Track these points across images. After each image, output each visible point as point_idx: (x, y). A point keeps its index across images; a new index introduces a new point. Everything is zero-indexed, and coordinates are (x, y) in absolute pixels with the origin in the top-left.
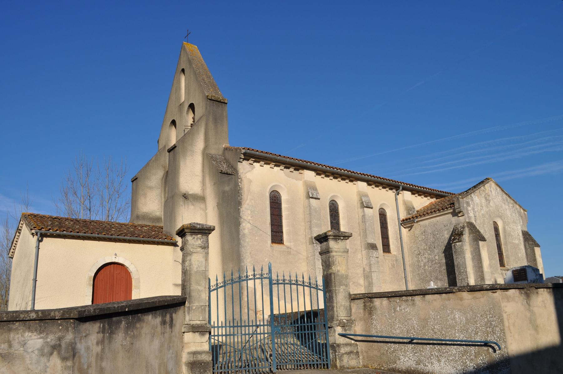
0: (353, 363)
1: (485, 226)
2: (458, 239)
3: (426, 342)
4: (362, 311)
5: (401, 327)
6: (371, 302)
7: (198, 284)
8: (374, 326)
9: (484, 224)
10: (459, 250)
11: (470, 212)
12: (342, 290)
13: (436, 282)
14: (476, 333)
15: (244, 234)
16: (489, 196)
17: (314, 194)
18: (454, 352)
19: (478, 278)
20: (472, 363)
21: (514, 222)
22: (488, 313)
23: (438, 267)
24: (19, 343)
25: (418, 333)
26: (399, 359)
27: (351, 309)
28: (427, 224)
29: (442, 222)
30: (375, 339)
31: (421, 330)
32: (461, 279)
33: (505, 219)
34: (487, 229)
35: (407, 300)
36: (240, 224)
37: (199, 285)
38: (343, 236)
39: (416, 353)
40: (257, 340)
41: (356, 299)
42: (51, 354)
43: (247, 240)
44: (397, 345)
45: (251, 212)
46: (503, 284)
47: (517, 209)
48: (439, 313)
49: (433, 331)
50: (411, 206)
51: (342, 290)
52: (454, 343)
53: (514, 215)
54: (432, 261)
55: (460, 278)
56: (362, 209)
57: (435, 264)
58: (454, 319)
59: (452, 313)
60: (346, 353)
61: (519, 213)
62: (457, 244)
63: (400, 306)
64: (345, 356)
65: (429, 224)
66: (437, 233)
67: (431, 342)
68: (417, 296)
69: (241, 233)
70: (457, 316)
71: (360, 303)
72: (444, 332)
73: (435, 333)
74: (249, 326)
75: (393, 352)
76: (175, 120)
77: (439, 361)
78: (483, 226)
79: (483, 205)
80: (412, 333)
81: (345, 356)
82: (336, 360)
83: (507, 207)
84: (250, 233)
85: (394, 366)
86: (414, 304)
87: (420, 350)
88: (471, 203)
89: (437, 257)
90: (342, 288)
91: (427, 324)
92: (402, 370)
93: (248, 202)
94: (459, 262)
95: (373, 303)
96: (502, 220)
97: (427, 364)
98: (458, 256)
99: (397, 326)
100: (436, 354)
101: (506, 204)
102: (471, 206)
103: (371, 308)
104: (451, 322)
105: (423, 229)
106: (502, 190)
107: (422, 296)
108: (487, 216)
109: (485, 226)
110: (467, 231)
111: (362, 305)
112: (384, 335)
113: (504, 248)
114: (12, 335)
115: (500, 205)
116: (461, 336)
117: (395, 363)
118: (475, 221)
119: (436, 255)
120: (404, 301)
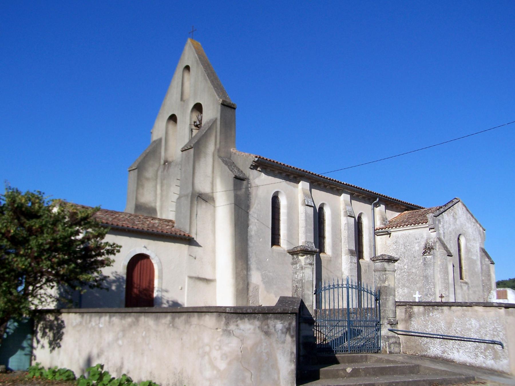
0: (396, 350)
1: (451, 242)
2: (429, 253)
3: (450, 338)
4: (403, 314)
5: (432, 327)
6: (411, 308)
7: (308, 289)
8: (413, 325)
9: (450, 240)
10: (429, 263)
11: (440, 229)
12: (391, 299)
13: (403, 289)
14: (486, 335)
15: (251, 236)
16: (456, 214)
17: (309, 201)
18: (470, 346)
19: (443, 289)
20: (481, 354)
21: (474, 240)
22: (495, 322)
23: (406, 276)
24: (272, 326)
25: (444, 332)
26: (430, 349)
27: (396, 312)
28: (400, 236)
29: (414, 235)
30: (412, 334)
31: (447, 330)
32: (428, 289)
33: (467, 236)
34: (452, 245)
35: (438, 309)
36: (248, 226)
37: (309, 291)
38: (393, 260)
39: (442, 345)
40: (339, 330)
41: (400, 306)
42: (286, 333)
43: (253, 241)
44: (428, 339)
45: (258, 215)
46: (52, 209)
47: (477, 227)
48: (460, 319)
49: (455, 331)
50: (384, 217)
51: (391, 299)
52: (469, 340)
53: (474, 233)
54: (401, 270)
55: (427, 288)
56: (345, 217)
57: (403, 273)
58: (471, 324)
59: (470, 320)
60: (392, 343)
61: (479, 231)
62: (428, 256)
63: (432, 313)
64: (392, 344)
65: (401, 235)
66: (408, 244)
67: (454, 338)
68: (445, 307)
69: (249, 235)
70: (473, 323)
71: (403, 309)
72: (463, 333)
73: (457, 333)
74: (334, 320)
75: (425, 344)
76: (177, 115)
77: (458, 352)
78: (450, 242)
79: (451, 223)
80: (440, 332)
81: (392, 344)
82: (386, 347)
83: (470, 226)
84: (256, 234)
85: (426, 353)
86: (442, 312)
87: (445, 344)
88: (441, 221)
89: (406, 267)
90: (391, 298)
91: (451, 326)
92: (431, 356)
93: (255, 205)
94: (427, 273)
95: (412, 309)
96: (465, 237)
97: (449, 353)
98: (427, 268)
99: (430, 326)
100: (457, 347)
101: (469, 222)
102: (442, 223)
103: (410, 313)
104: (468, 326)
105: (396, 240)
106: (467, 210)
107: (449, 307)
108: (453, 233)
109: (451, 242)
110: (438, 245)
111: (404, 310)
112: (419, 331)
113: (465, 262)
114: (269, 321)
115: (464, 224)
116: (475, 336)
117: (427, 351)
118: (444, 237)
119: (405, 265)
120: (436, 309)
